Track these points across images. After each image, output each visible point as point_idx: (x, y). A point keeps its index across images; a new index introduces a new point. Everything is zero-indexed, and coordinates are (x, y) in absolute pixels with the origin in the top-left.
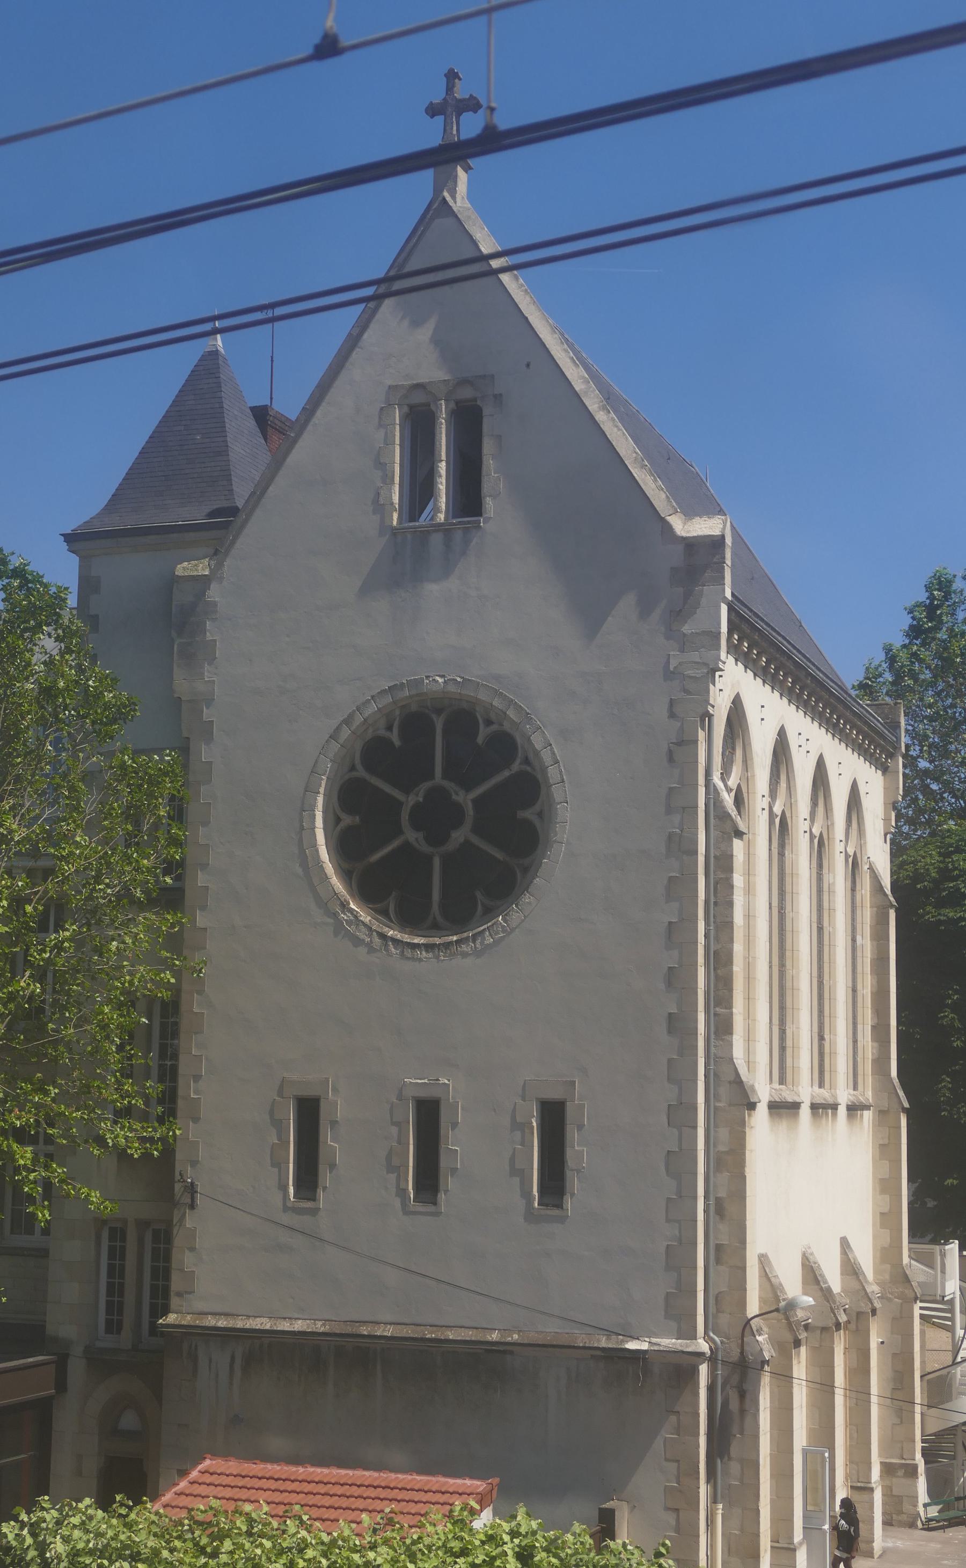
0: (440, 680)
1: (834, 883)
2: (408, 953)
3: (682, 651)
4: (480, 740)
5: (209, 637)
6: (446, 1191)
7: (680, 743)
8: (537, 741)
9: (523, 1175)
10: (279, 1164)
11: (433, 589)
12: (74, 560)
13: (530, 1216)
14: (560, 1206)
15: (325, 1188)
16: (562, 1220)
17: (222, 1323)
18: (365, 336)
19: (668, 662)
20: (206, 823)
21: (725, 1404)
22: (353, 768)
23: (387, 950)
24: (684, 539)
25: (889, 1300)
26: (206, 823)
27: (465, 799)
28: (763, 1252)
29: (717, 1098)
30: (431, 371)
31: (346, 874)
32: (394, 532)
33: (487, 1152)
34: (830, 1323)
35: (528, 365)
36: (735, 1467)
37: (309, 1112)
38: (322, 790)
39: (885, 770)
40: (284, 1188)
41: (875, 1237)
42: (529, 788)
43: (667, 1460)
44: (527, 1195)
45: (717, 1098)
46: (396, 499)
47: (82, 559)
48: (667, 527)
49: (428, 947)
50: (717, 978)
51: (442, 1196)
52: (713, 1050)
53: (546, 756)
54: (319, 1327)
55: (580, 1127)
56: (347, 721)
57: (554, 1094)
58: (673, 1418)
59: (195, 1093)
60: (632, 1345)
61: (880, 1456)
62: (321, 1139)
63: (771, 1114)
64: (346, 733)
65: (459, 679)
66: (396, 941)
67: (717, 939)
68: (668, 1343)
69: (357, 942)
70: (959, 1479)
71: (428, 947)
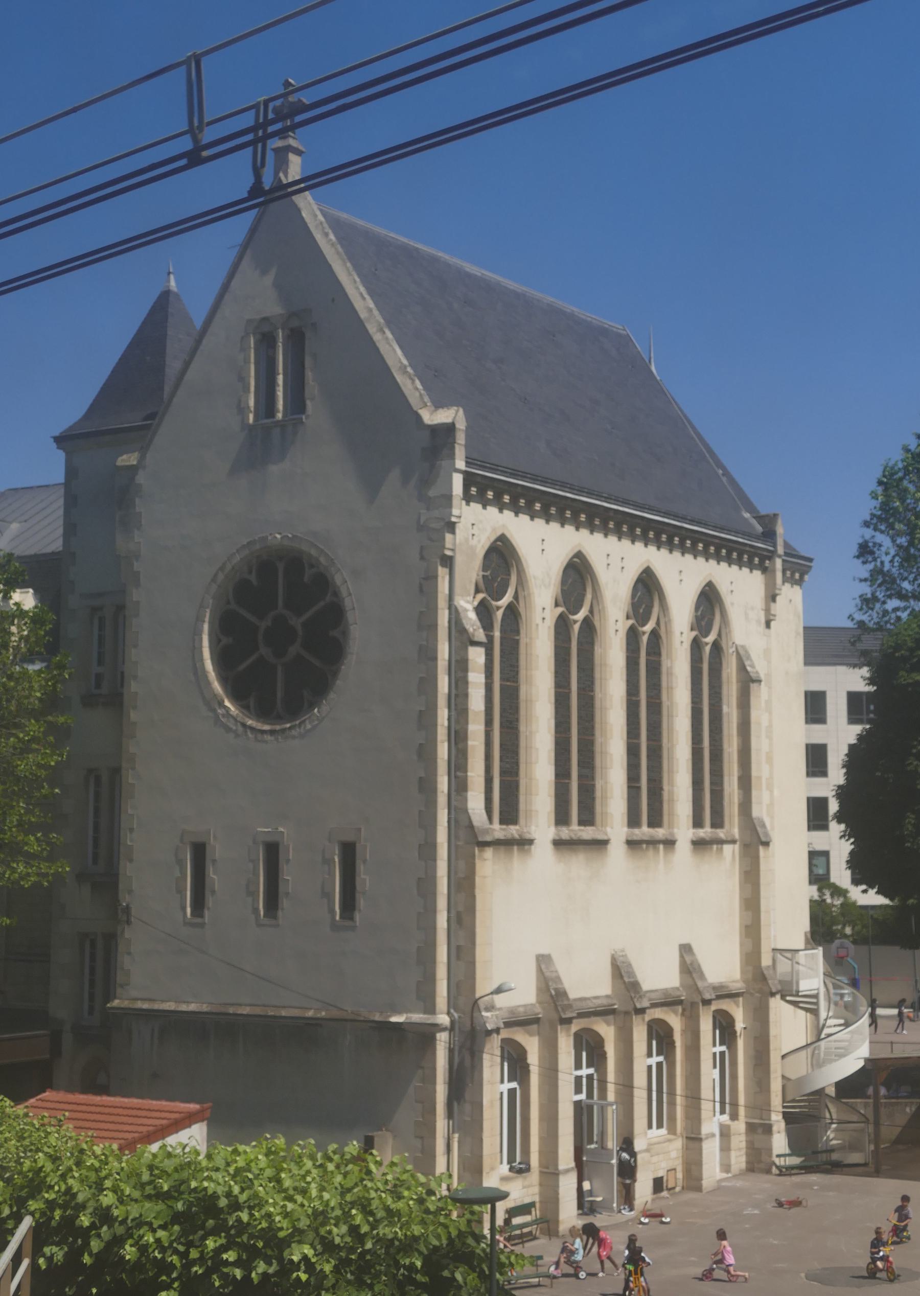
0: (278, 536)
1: (671, 667)
2: (259, 736)
3: (428, 509)
4: (306, 579)
5: (137, 510)
6: (283, 909)
7: (426, 578)
8: (338, 580)
9: (329, 896)
10: (181, 891)
11: (274, 469)
12: (61, 455)
13: (334, 927)
14: (352, 919)
15: (209, 909)
16: (353, 928)
17: (146, 1006)
18: (232, 284)
19: (419, 518)
20: (135, 646)
21: (461, 1063)
22: (228, 603)
23: (246, 735)
24: (429, 426)
25: (752, 994)
26: (135, 646)
27: (297, 622)
28: (544, 951)
29: (457, 838)
30: (274, 309)
31: (223, 680)
32: (251, 428)
33: (309, 879)
34: (630, 1008)
35: (333, 300)
36: (467, 1107)
37: (200, 852)
38: (207, 619)
39: (764, 570)
40: (184, 909)
41: (741, 945)
42: (335, 614)
43: (416, 1101)
44: (332, 911)
45: (457, 838)
46: (252, 403)
47: (67, 454)
48: (419, 418)
49: (272, 732)
50: (458, 750)
51: (280, 913)
52: (453, 803)
53: (344, 592)
54: (205, 1008)
55: (365, 861)
56: (222, 569)
57: (349, 838)
58: (420, 1071)
59: (131, 841)
60: (394, 1019)
61: (746, 1117)
62: (207, 873)
63: (694, 849)
64: (221, 577)
65: (290, 536)
66: (252, 729)
67: (457, 722)
68: (417, 1017)
69: (228, 730)
70: (822, 1138)
71: (272, 732)
